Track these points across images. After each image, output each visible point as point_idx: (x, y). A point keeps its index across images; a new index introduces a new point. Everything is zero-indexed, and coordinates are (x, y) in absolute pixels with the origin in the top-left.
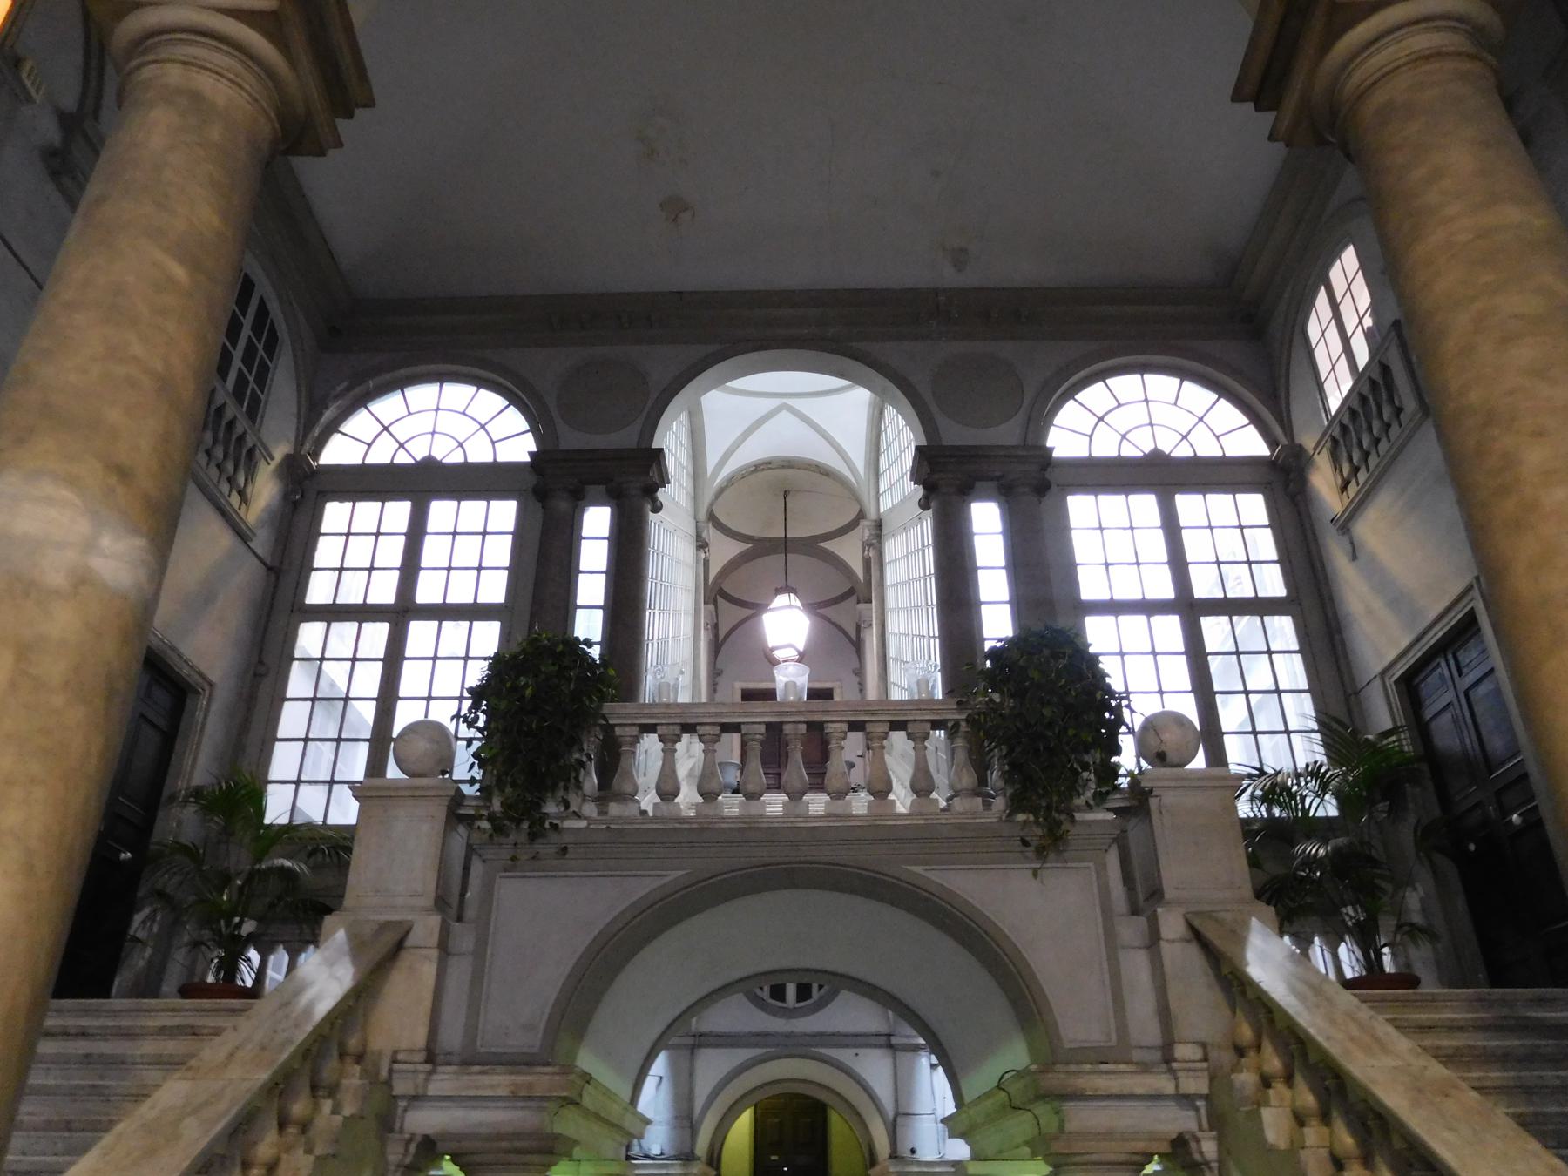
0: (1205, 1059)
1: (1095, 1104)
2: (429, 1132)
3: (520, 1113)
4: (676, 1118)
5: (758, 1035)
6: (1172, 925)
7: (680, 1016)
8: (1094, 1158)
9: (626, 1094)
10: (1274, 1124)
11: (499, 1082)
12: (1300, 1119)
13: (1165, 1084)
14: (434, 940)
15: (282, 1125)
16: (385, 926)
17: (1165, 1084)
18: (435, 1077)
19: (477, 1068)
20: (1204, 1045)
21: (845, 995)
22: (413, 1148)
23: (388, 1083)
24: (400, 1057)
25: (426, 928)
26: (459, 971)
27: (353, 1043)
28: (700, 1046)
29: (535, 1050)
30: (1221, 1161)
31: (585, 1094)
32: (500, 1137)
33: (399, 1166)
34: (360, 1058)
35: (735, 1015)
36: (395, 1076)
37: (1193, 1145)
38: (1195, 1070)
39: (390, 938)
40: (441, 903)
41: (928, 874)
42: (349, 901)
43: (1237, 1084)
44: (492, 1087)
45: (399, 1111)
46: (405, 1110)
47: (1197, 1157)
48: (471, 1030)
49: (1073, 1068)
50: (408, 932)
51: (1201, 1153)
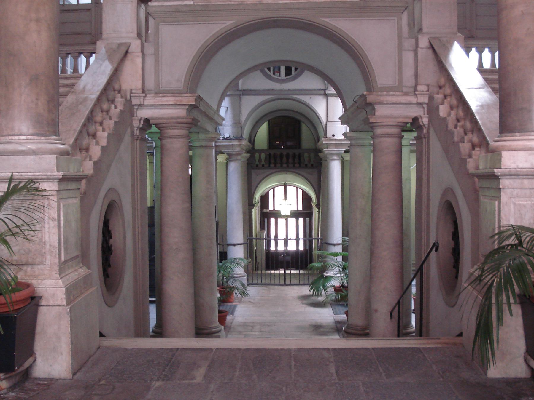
0: (428, 91)
1: (387, 106)
2: (146, 117)
3: (177, 111)
4: (235, 123)
5: (268, 90)
6: (424, 42)
7: (235, 79)
8: (385, 124)
9: (215, 107)
10: (443, 110)
11: (170, 100)
12: (452, 108)
13: (413, 99)
14: (139, 50)
15: (102, 111)
16: (120, 45)
17: (413, 99)
18: (146, 98)
19: (160, 95)
20: (428, 86)
21: (307, 74)
22: (142, 122)
23: (130, 101)
24: (133, 91)
25: (135, 45)
26: (150, 62)
27: (117, 86)
28: (243, 95)
29: (182, 89)
30: (429, 125)
31: (201, 105)
32: (172, 118)
33: (138, 128)
34: (119, 92)
35: (258, 81)
36: (132, 98)
37: (420, 119)
38: (424, 94)
39: (123, 50)
40: (139, 35)
41: (332, 22)
42: (104, 35)
43: (436, 98)
44: (167, 101)
45: (135, 110)
46: (137, 110)
47: (421, 124)
48: (157, 84)
49: (379, 93)
50: (129, 46)
51: (422, 122)
